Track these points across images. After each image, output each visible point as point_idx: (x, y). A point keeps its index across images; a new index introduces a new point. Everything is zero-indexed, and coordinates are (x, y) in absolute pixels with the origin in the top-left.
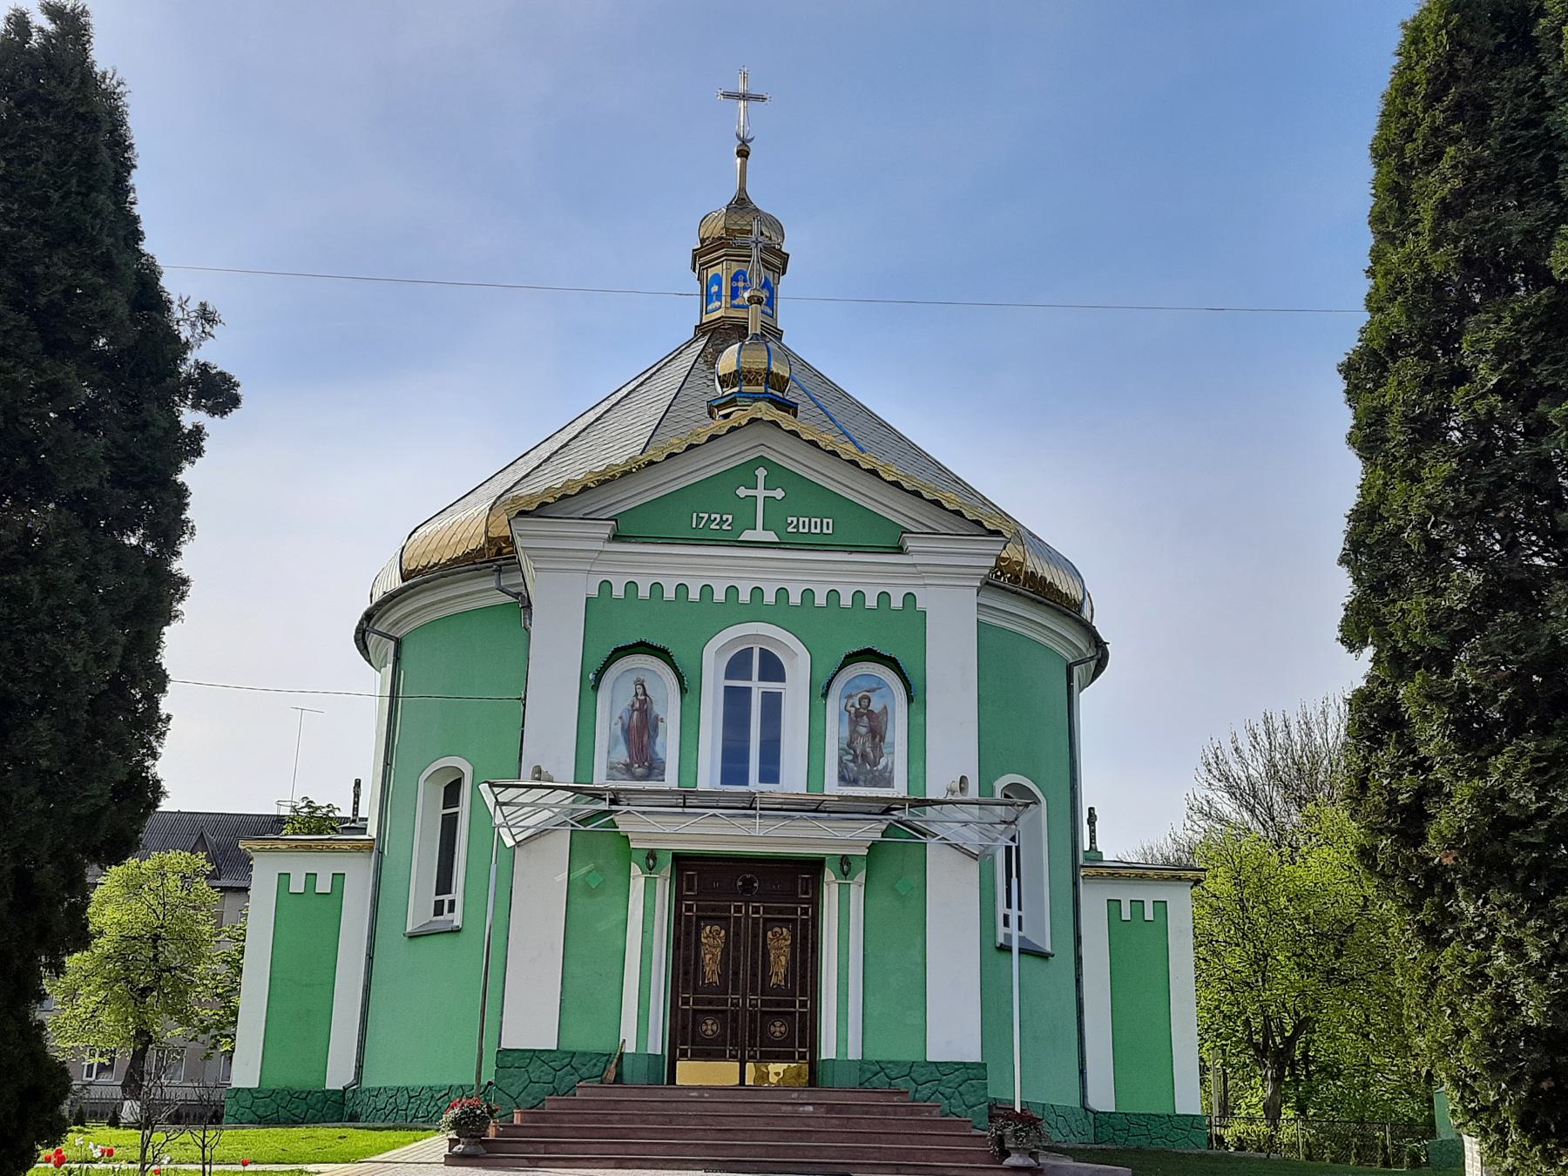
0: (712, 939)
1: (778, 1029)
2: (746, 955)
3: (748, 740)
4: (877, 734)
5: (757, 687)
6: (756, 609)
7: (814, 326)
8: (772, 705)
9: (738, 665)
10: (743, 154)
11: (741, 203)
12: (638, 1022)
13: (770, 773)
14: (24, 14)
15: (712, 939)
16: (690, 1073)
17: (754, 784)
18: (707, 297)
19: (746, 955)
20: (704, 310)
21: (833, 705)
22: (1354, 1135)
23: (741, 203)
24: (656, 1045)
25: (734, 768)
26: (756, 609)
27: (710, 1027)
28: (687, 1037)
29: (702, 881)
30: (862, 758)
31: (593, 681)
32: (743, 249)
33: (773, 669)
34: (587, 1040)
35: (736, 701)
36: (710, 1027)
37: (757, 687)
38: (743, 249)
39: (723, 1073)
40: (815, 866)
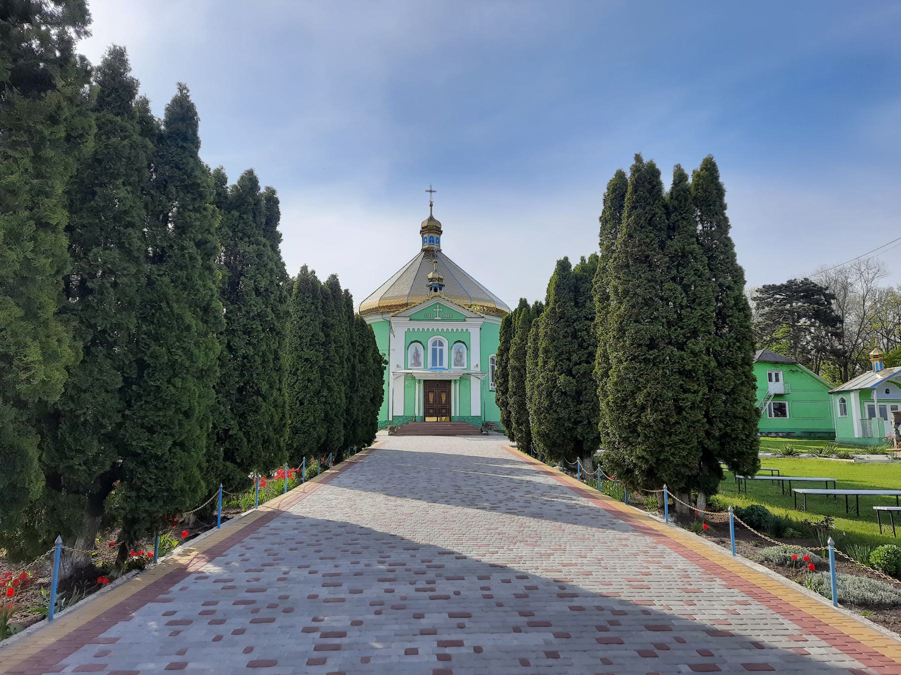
0: (431, 396)
1: (444, 411)
2: (438, 398)
3: (437, 357)
4: (461, 356)
5: (438, 348)
6: (438, 333)
7: (448, 246)
8: (441, 351)
9: (434, 344)
10: (431, 206)
11: (431, 218)
12: (418, 410)
13: (441, 364)
14: (274, 192)
15: (431, 396)
16: (428, 419)
17: (438, 366)
18: (424, 242)
19: (438, 398)
20: (423, 245)
21: (453, 351)
22: (677, 423)
23: (431, 218)
24: (422, 414)
25: (434, 363)
26: (438, 333)
27: (431, 411)
28: (427, 413)
29: (429, 385)
30: (458, 362)
31: (407, 348)
32: (432, 230)
33: (441, 344)
34: (409, 414)
35: (434, 351)
36: (431, 411)
37: (438, 348)
38: (432, 230)
39: (434, 419)
40: (450, 381)
